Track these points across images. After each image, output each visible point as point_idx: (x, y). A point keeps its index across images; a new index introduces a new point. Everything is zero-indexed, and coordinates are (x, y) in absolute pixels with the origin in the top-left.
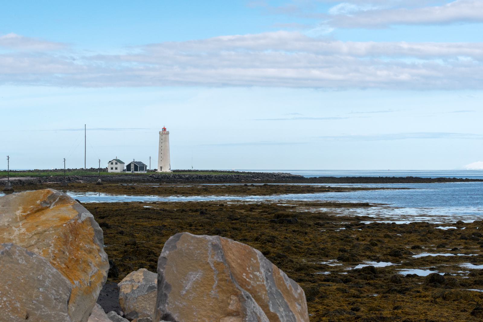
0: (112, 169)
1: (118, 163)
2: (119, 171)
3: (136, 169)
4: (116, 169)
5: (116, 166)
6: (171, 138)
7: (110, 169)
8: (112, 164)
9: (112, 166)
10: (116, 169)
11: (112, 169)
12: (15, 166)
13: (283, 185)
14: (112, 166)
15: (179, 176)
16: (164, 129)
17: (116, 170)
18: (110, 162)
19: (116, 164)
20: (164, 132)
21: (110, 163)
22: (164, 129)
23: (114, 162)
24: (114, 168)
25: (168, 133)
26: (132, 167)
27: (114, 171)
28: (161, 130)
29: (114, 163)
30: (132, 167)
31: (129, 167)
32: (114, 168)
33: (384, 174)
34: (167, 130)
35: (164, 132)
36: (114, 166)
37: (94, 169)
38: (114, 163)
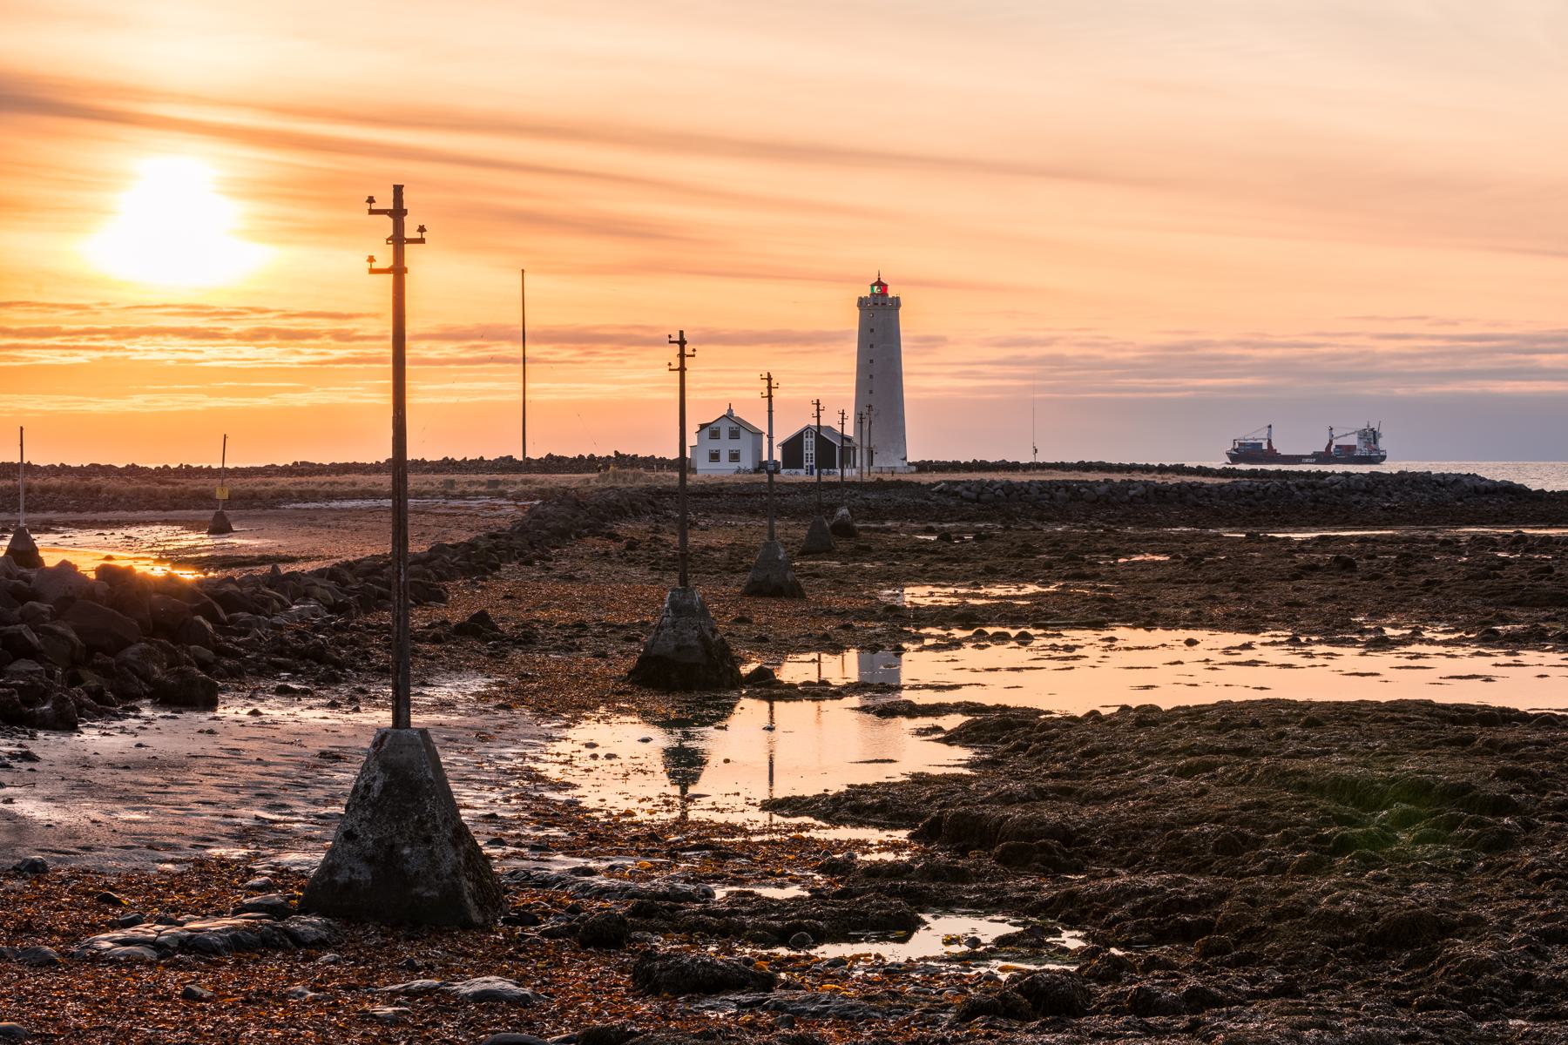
5: (734, 445)
7: (742, 457)
8: (715, 435)
9: (714, 445)
10: (735, 457)
11: (715, 457)
12: (39, 457)
13: (1548, 539)
14: (714, 445)
15: (1067, 489)
17: (715, 465)
20: (879, 314)
21: (707, 431)
26: (809, 449)
29: (724, 433)
30: (809, 449)
31: (793, 448)
33: (639, 376)
35: (879, 314)
36: (725, 445)
37: (561, 459)
38: (724, 433)
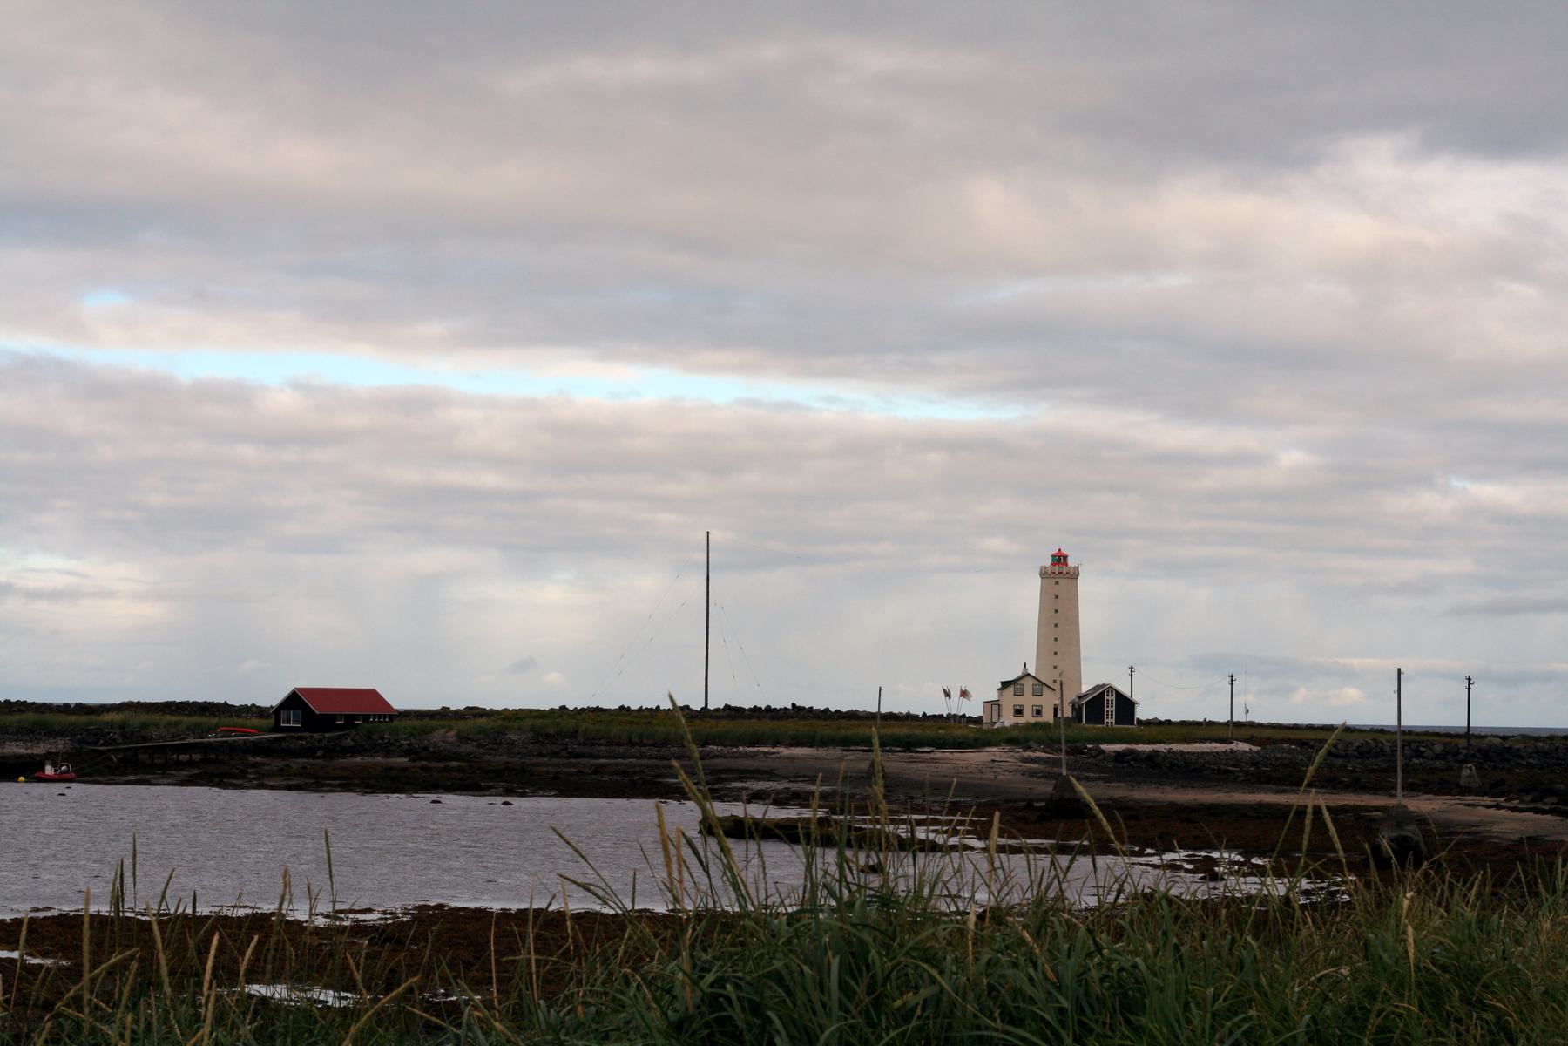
5: (1038, 701)
6: (1087, 587)
9: (1019, 701)
16: (1060, 559)
18: (1005, 685)
21: (1011, 690)
22: (1060, 559)
25: (1074, 575)
26: (1110, 709)
28: (1048, 562)
30: (1110, 709)
34: (1071, 562)
37: (739, 710)
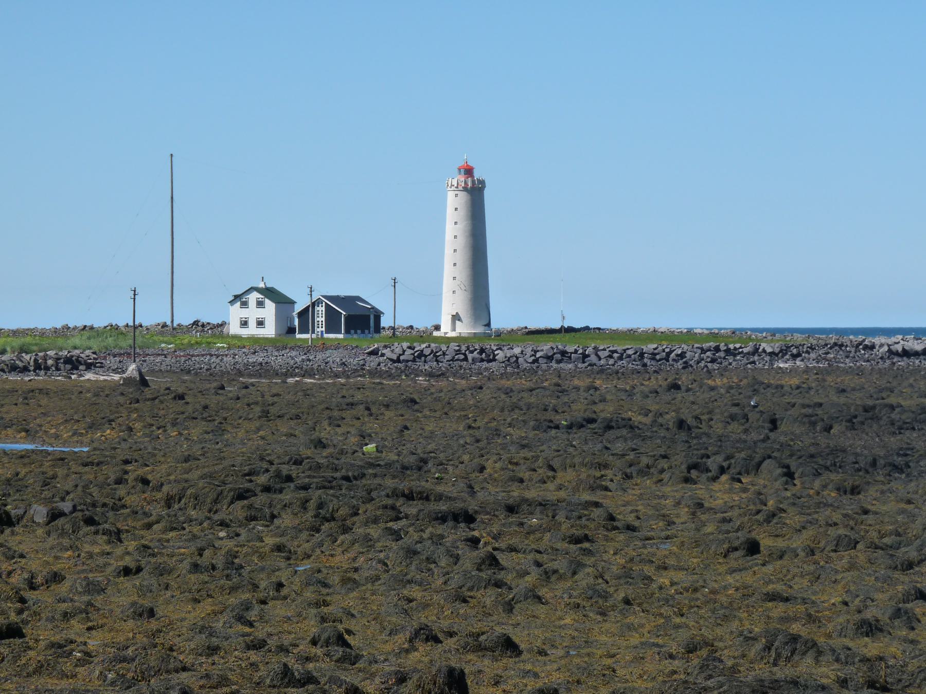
0: (244, 324)
1: (267, 301)
2: (269, 331)
3: (332, 326)
4: (260, 323)
9: (244, 313)
10: (260, 323)
11: (244, 324)
14: (244, 313)
19: (260, 304)
23: (254, 297)
24: (252, 323)
27: (253, 330)
32: (252, 323)
